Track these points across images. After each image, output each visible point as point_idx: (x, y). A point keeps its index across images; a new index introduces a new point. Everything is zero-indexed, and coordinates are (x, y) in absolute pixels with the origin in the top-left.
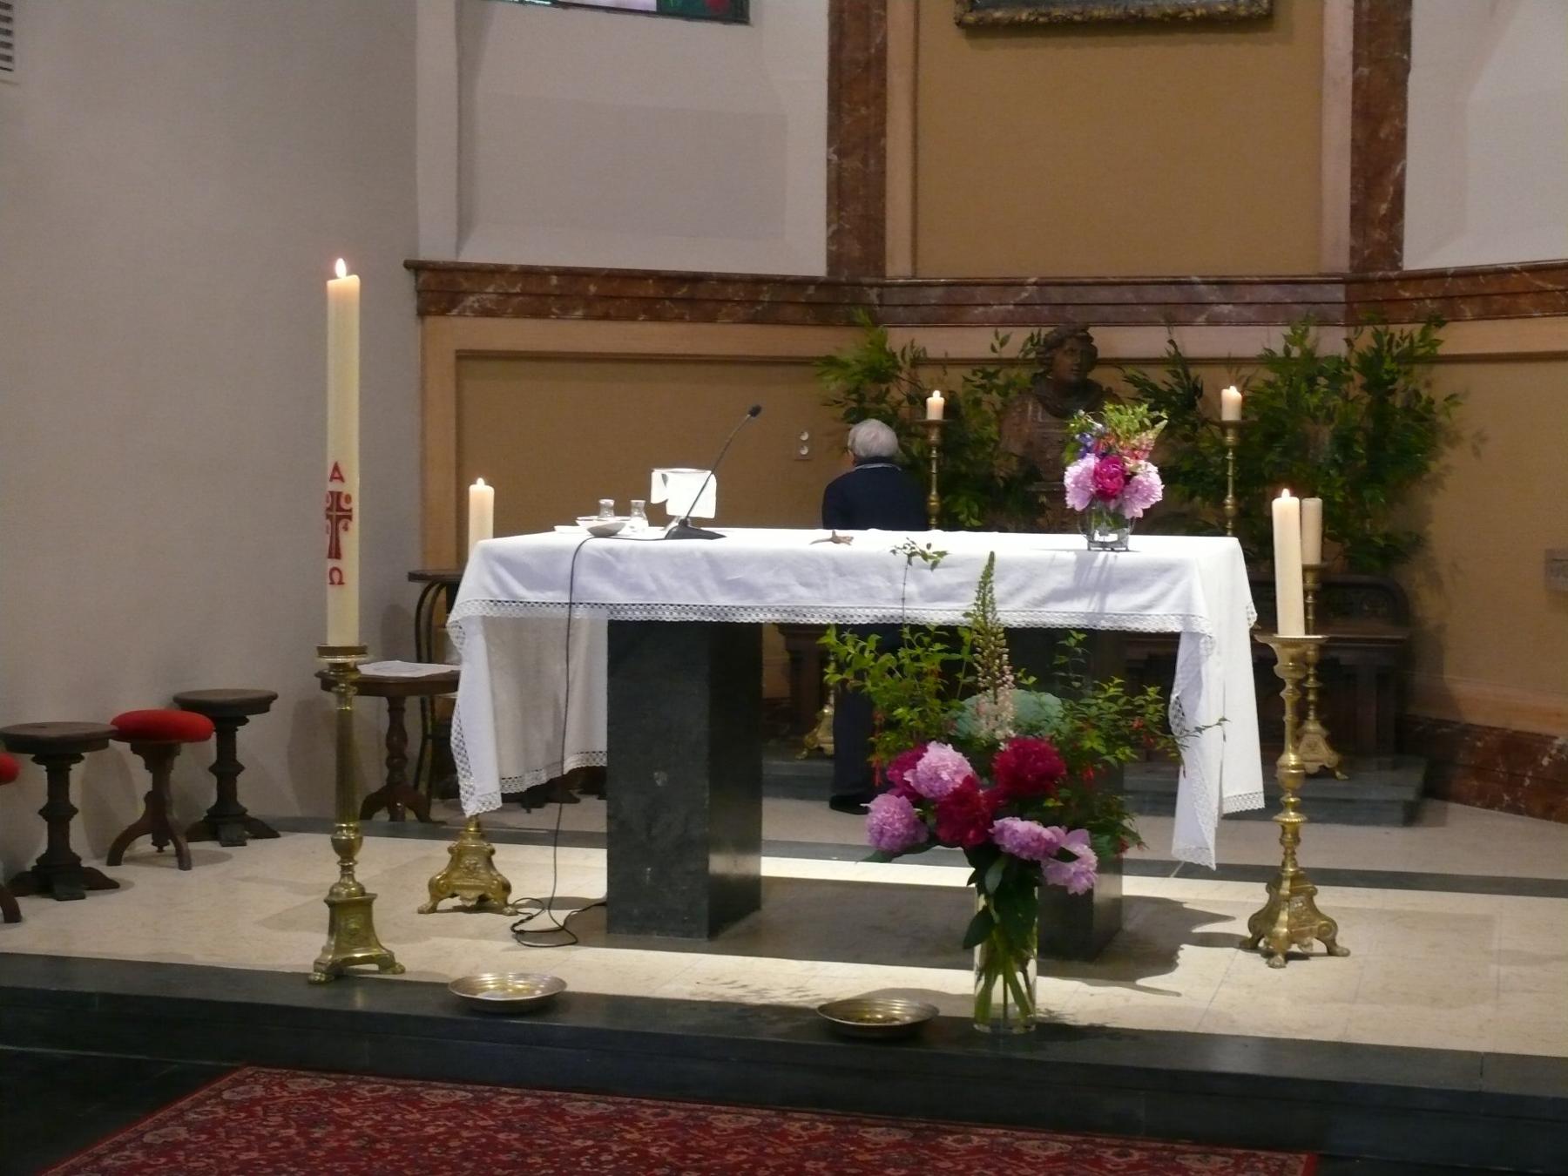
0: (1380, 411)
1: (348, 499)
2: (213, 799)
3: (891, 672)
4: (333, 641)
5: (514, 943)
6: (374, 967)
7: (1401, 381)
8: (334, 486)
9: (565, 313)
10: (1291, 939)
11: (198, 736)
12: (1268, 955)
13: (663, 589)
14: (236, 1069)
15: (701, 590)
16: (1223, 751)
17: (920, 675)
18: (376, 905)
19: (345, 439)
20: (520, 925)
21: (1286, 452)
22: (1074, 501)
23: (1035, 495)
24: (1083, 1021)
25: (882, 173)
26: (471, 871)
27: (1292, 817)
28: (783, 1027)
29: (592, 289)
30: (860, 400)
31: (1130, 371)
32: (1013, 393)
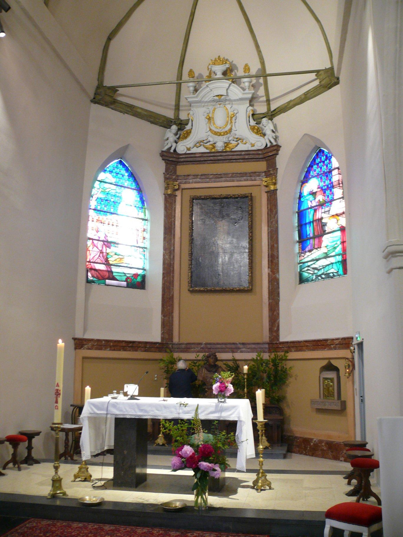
0: (276, 371)
1: (60, 391)
2: (26, 455)
3: (176, 430)
4: (55, 422)
5: (92, 489)
6: (61, 495)
7: (280, 365)
8: (57, 388)
9: (106, 349)
10: (262, 486)
11: (24, 441)
12: (257, 490)
13: (127, 411)
14: (29, 519)
15: (135, 411)
16: (247, 445)
17: (183, 430)
18: (62, 481)
19: (60, 378)
20: (93, 485)
21: (257, 379)
22: (215, 392)
23: (205, 389)
24: (218, 506)
25: (173, 321)
26: (83, 472)
27: (261, 459)
28: (152, 509)
29: (112, 344)
30: (168, 368)
31: (224, 362)
32: (200, 367)
